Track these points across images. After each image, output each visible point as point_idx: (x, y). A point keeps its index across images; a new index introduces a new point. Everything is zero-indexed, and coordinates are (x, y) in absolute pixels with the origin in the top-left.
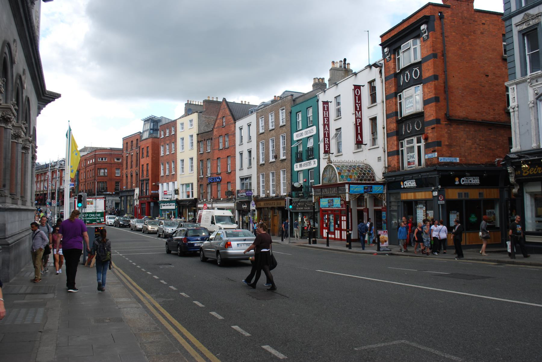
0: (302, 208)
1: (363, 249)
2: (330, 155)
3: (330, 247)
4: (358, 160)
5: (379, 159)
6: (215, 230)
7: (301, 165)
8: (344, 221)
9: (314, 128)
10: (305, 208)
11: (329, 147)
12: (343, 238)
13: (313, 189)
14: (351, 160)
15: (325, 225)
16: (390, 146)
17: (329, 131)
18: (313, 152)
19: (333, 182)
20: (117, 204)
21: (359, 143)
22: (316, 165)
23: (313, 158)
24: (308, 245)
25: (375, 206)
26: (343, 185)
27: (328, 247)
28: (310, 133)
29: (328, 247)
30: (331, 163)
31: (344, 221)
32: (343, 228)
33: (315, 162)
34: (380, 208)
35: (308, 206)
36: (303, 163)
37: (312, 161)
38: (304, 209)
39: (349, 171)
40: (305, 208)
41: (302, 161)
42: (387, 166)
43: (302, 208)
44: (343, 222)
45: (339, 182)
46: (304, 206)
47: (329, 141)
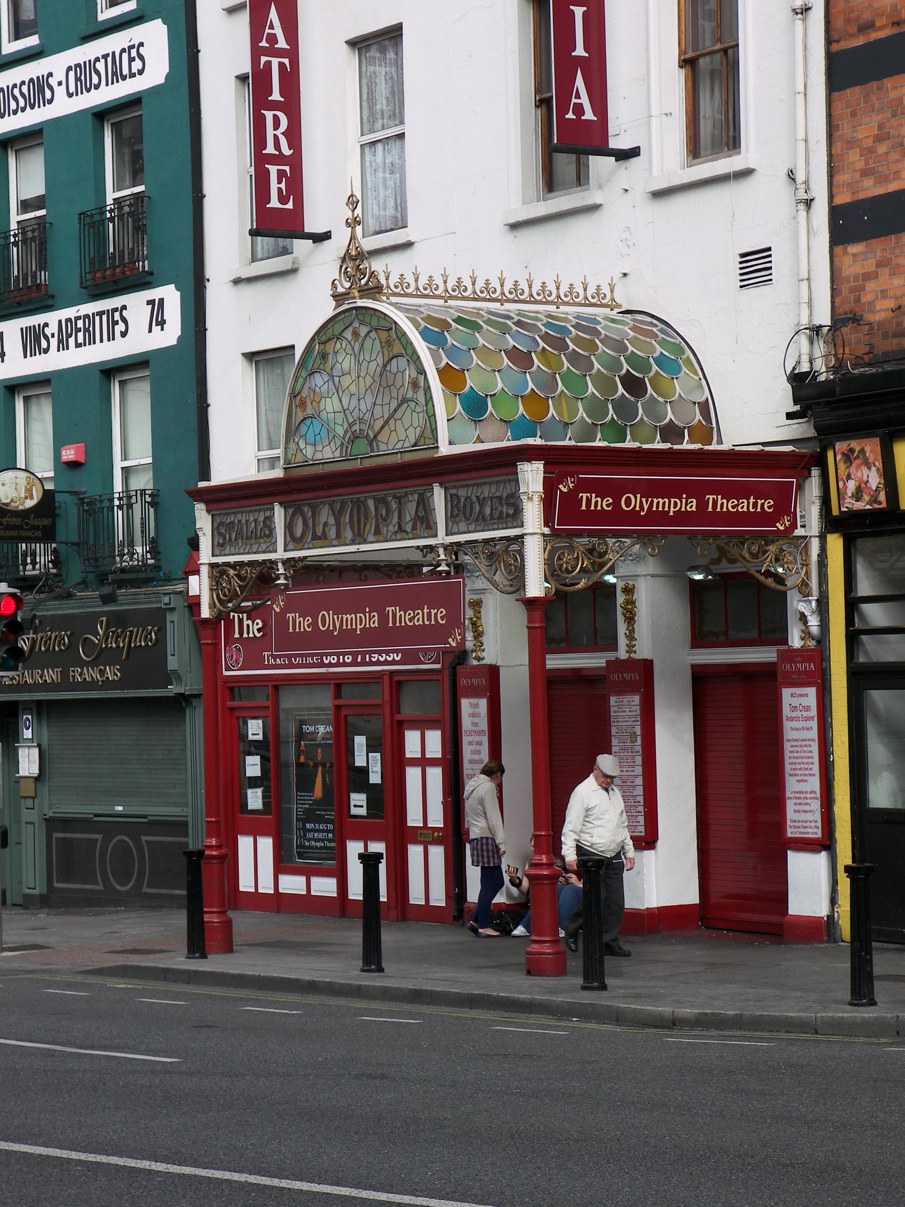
0: (51, 675)
1: (594, 978)
2: (301, 246)
3: (397, 975)
4: (544, 276)
5: (755, 266)
6: (619, 840)
7: (34, 341)
8: (423, 762)
9: (154, 37)
10: (77, 674)
11: (294, 185)
12: (416, 896)
13: (203, 521)
14: (488, 273)
15: (358, 802)
16: (854, 157)
17: (293, 54)
18: (140, 229)
19: (398, 442)
20: (880, 127)
21: (571, 139)
22: (170, 335)
23: (143, 282)
24: (180, 961)
25: (699, 639)
26: (503, 462)
27: (372, 980)
28: (117, 76)
29: (372, 980)
30: (375, 290)
31: (423, 762)
32: (414, 819)
33: (158, 306)
34: (765, 655)
35: (101, 657)
36: (52, 319)
37: (136, 304)
38: (65, 684)
39: (521, 359)
40: (77, 674)
41: (44, 302)
42: (824, 318)
43: (51, 675)
44: (413, 775)
45: (445, 449)
46: (65, 659)
47: (294, 135)
